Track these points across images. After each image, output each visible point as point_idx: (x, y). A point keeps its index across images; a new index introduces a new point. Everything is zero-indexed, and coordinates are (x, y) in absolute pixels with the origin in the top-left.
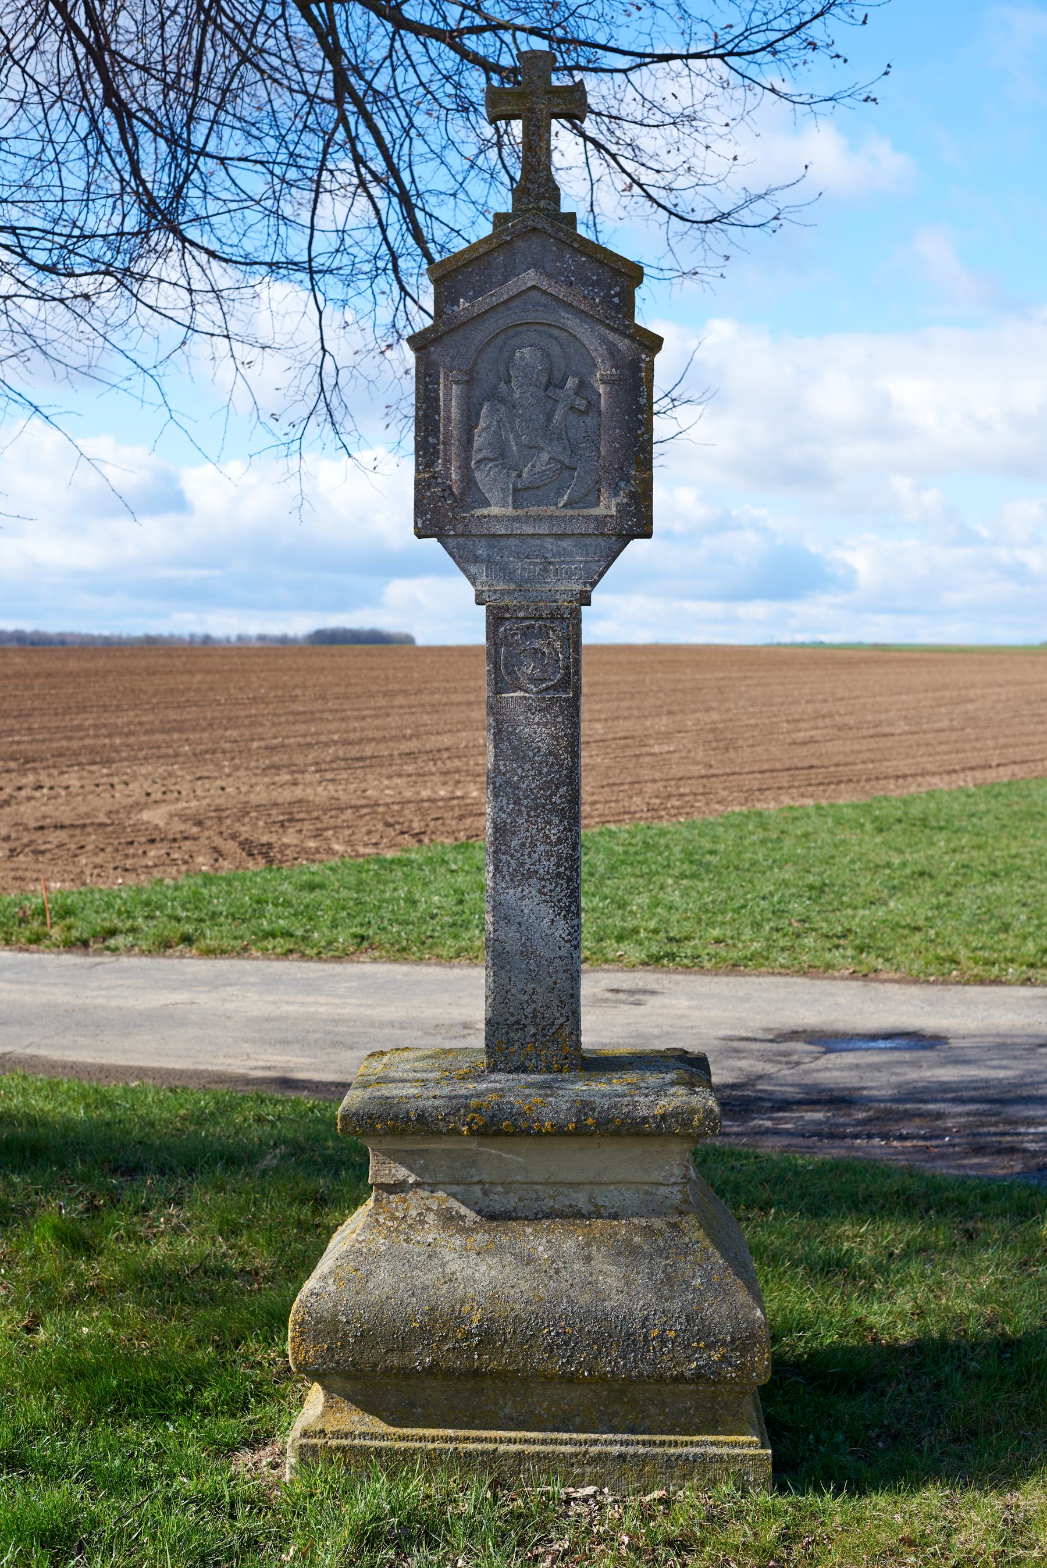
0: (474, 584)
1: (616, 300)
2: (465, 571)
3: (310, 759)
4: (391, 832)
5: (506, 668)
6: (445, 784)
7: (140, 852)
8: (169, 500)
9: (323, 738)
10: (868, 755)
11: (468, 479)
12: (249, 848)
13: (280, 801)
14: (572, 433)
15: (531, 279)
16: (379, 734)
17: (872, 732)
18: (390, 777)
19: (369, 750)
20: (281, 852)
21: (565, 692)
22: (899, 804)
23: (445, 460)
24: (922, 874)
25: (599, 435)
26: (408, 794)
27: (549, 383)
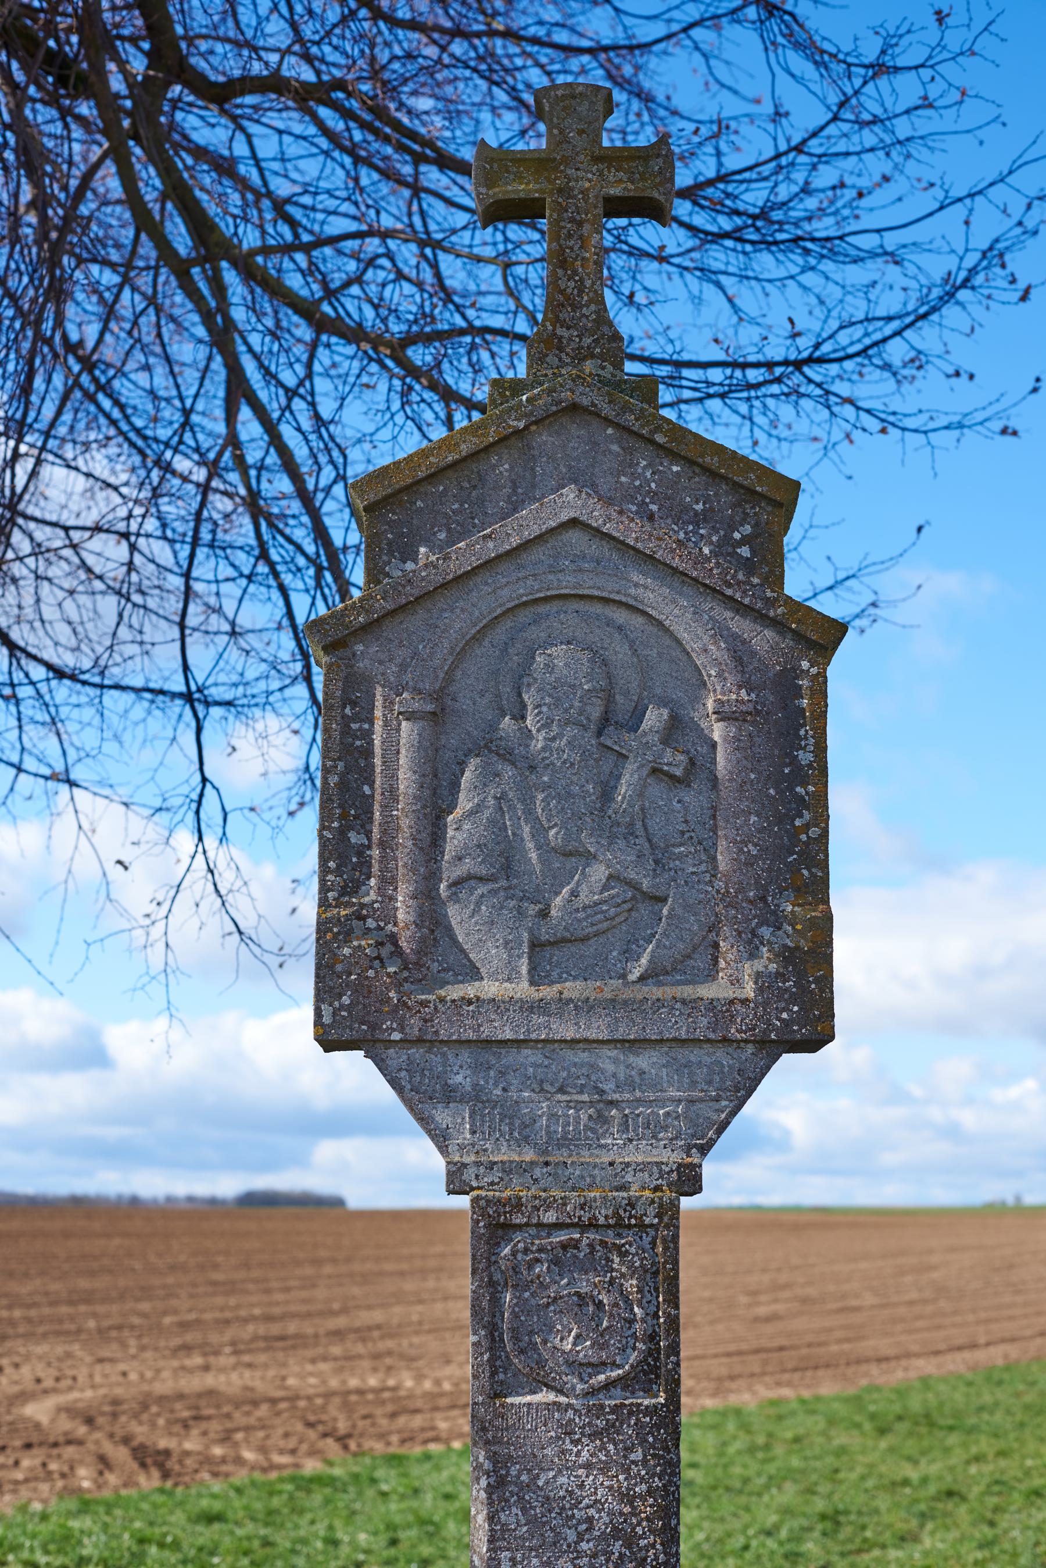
0: (443, 1149)
1: (745, 551)
2: (424, 1121)
3: (227, 1336)
4: (312, 1434)
5: (516, 1339)
6: (375, 1370)
7: (11, 1461)
8: (88, 1054)
9: (243, 1313)
10: (839, 1334)
11: (432, 921)
12: (146, 1457)
13: (187, 1391)
14: (655, 823)
15: (569, 505)
16: (303, 1308)
17: (839, 1305)
18: (313, 1361)
19: (292, 1328)
20: (180, 1462)
21: (649, 1392)
22: (893, 1396)
23: (383, 879)
24: (950, 1494)
25: (714, 830)
26: (334, 1383)
27: (605, 721)
